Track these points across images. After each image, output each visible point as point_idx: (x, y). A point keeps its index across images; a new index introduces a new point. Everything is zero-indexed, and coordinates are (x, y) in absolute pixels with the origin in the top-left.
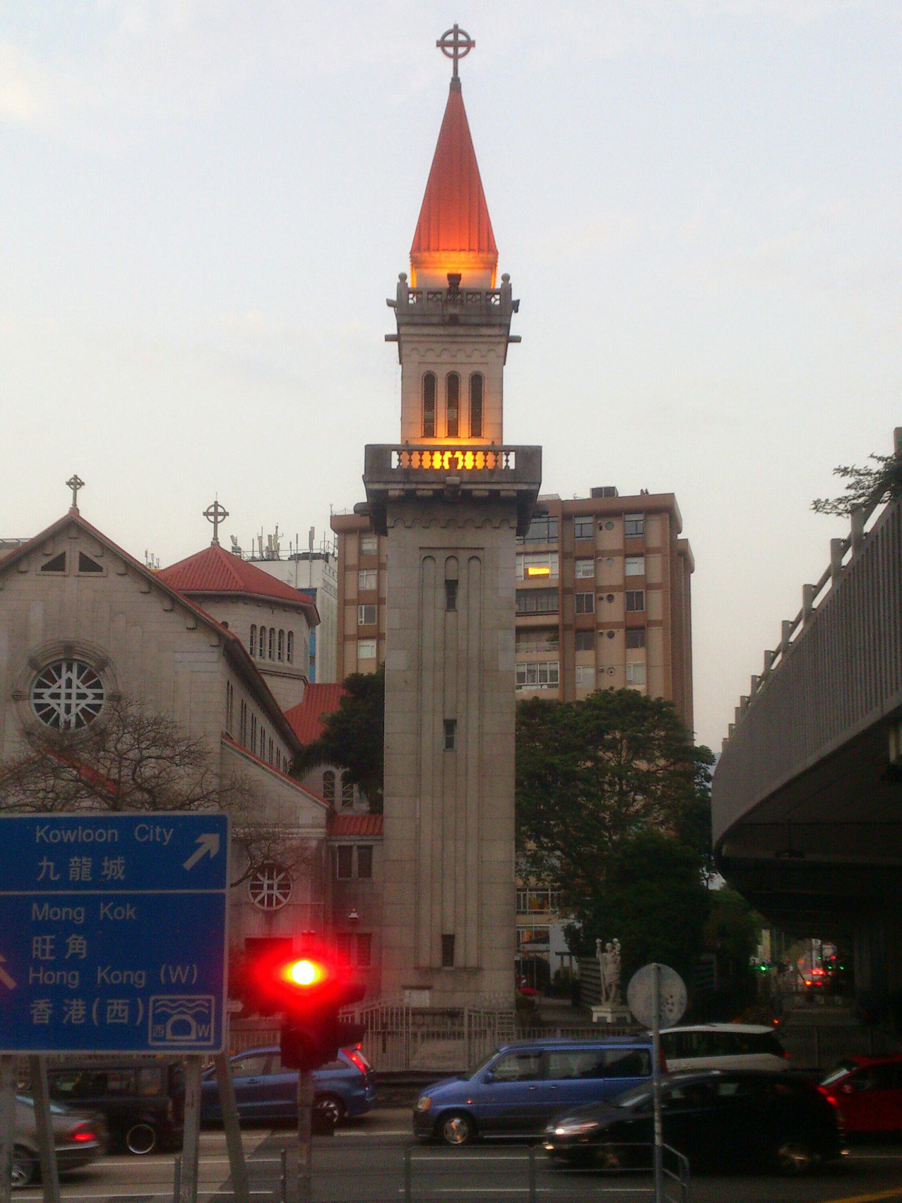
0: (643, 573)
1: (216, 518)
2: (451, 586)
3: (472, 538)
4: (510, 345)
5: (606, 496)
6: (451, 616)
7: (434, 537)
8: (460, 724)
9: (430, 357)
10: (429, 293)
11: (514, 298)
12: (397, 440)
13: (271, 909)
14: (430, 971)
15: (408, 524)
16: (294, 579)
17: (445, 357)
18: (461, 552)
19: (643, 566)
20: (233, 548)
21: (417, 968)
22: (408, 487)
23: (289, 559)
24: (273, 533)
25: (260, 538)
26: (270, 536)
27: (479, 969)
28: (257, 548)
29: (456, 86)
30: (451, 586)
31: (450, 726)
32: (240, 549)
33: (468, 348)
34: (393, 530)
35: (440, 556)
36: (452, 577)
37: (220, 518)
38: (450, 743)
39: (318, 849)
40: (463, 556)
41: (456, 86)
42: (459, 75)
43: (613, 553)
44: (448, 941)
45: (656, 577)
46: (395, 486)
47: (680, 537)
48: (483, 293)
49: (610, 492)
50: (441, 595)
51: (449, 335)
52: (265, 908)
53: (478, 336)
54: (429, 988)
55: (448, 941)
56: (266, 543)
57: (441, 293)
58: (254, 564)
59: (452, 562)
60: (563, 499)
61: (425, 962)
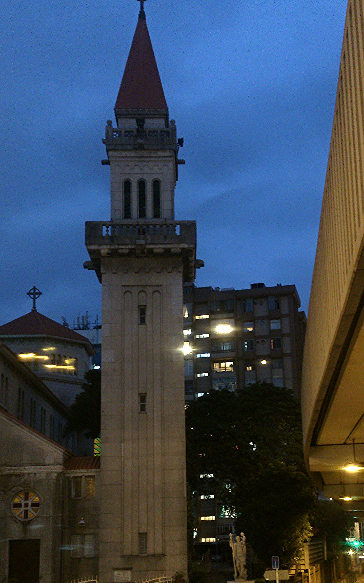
0: (279, 328)
1: (34, 296)
2: (142, 311)
3: (154, 279)
5: (259, 287)
6: (142, 327)
7: (131, 279)
8: (149, 395)
10: (125, 132)
11: (179, 136)
12: (107, 218)
13: (27, 520)
14: (130, 557)
15: (115, 271)
16: (96, 339)
17: (137, 170)
18: (148, 288)
19: (279, 324)
21: (123, 556)
23: (94, 329)
24: (85, 315)
25: (78, 318)
26: (83, 317)
27: (163, 555)
28: (76, 323)
29: (142, 16)
30: (142, 311)
31: (143, 398)
32: (67, 324)
34: (105, 275)
35: (135, 291)
36: (142, 304)
38: (143, 409)
39: (57, 479)
40: (150, 290)
41: (142, 16)
42: (145, 10)
43: (262, 318)
44: (143, 536)
45: (287, 330)
47: (300, 310)
49: (262, 285)
50: (136, 315)
51: (139, 157)
52: (23, 520)
53: (156, 157)
54: (130, 569)
58: (76, 331)
59: (143, 294)
60: (236, 290)
61: (127, 552)
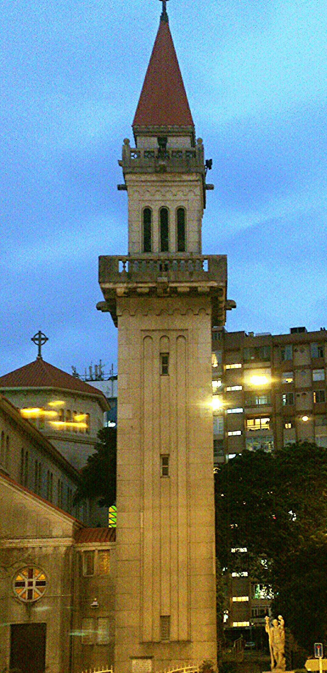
2: (165, 359)
3: (178, 323)
4: (207, 191)
5: (300, 332)
7: (151, 322)
9: (148, 196)
14: (151, 644)
17: (158, 197)
20: (73, 374)
21: (142, 643)
22: (130, 286)
24: (98, 364)
27: (189, 641)
28: (88, 373)
29: (164, 18)
30: (165, 359)
31: (165, 460)
32: (78, 374)
33: (174, 190)
34: (121, 318)
37: (43, 342)
38: (165, 472)
39: (66, 554)
40: (173, 335)
41: (164, 18)
42: (167, 11)
43: (304, 367)
44: (165, 619)
46: (121, 285)
48: (184, 152)
50: (157, 364)
54: (151, 658)
55: (165, 619)
56: (93, 371)
57: (153, 152)
61: (147, 638)
